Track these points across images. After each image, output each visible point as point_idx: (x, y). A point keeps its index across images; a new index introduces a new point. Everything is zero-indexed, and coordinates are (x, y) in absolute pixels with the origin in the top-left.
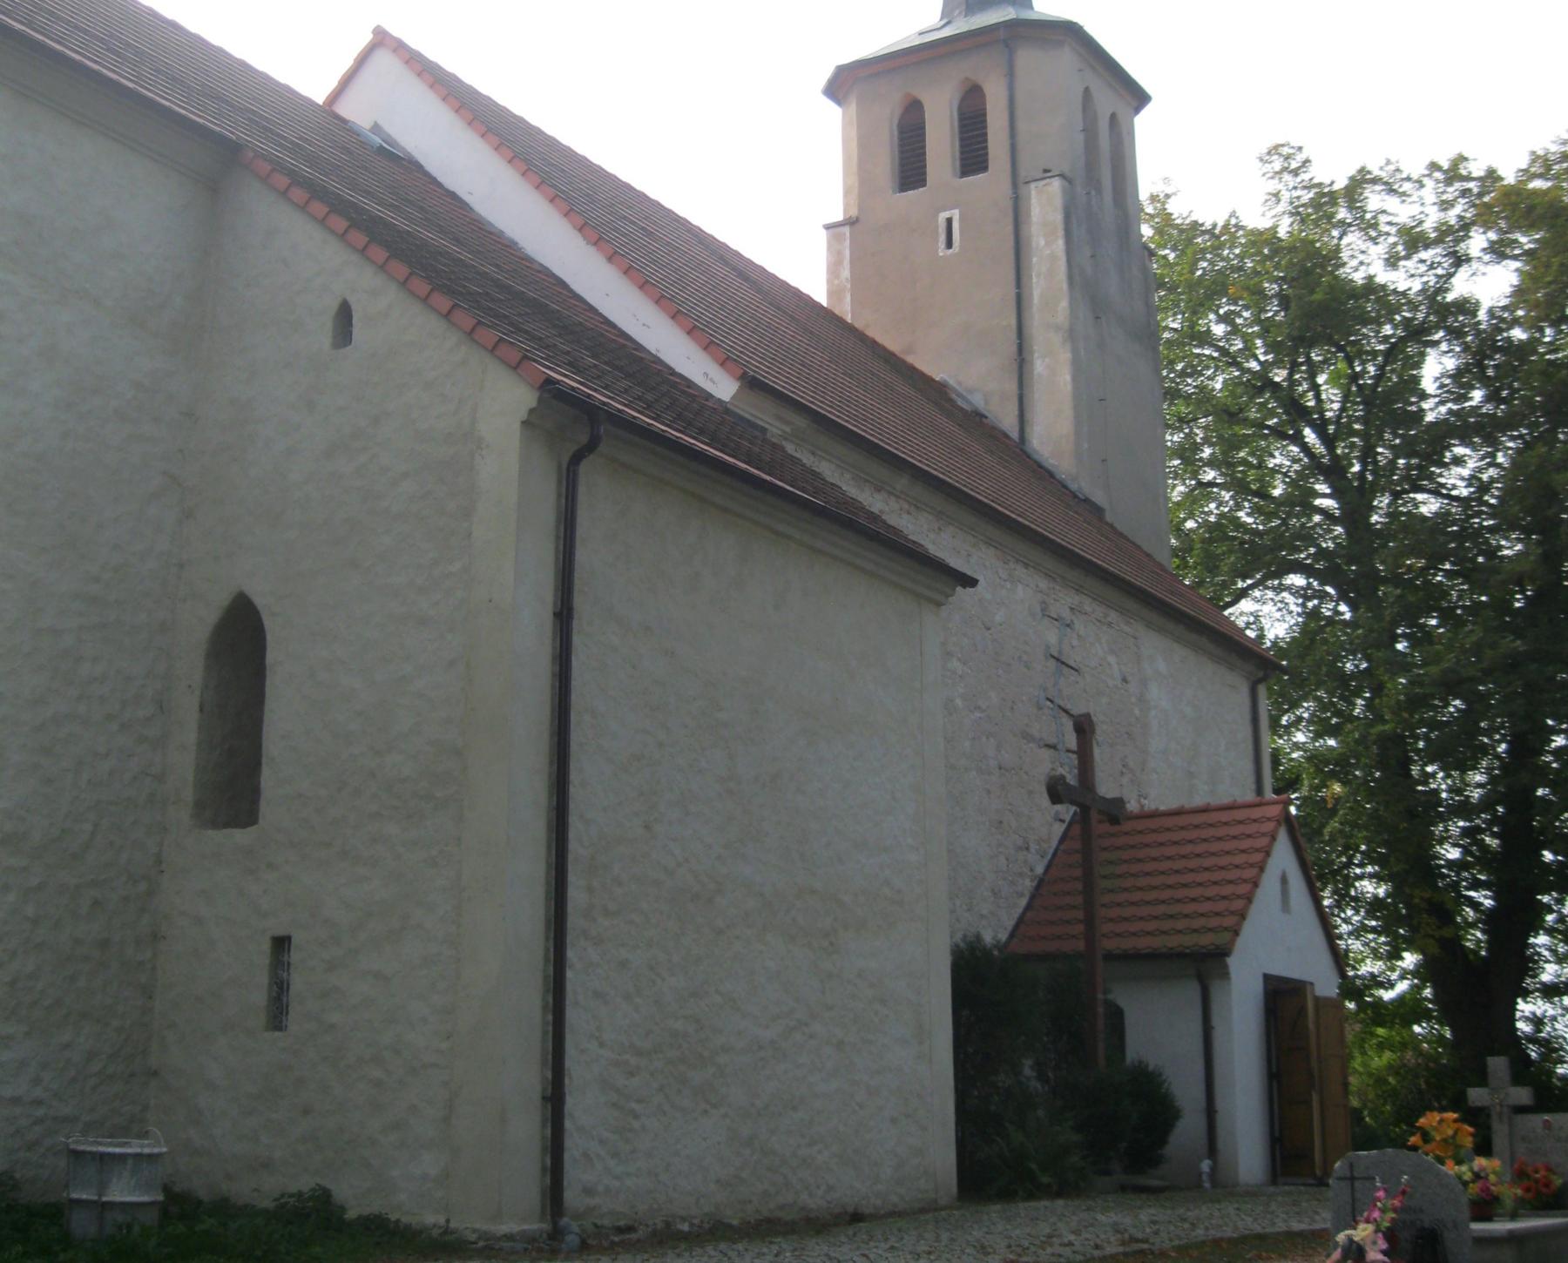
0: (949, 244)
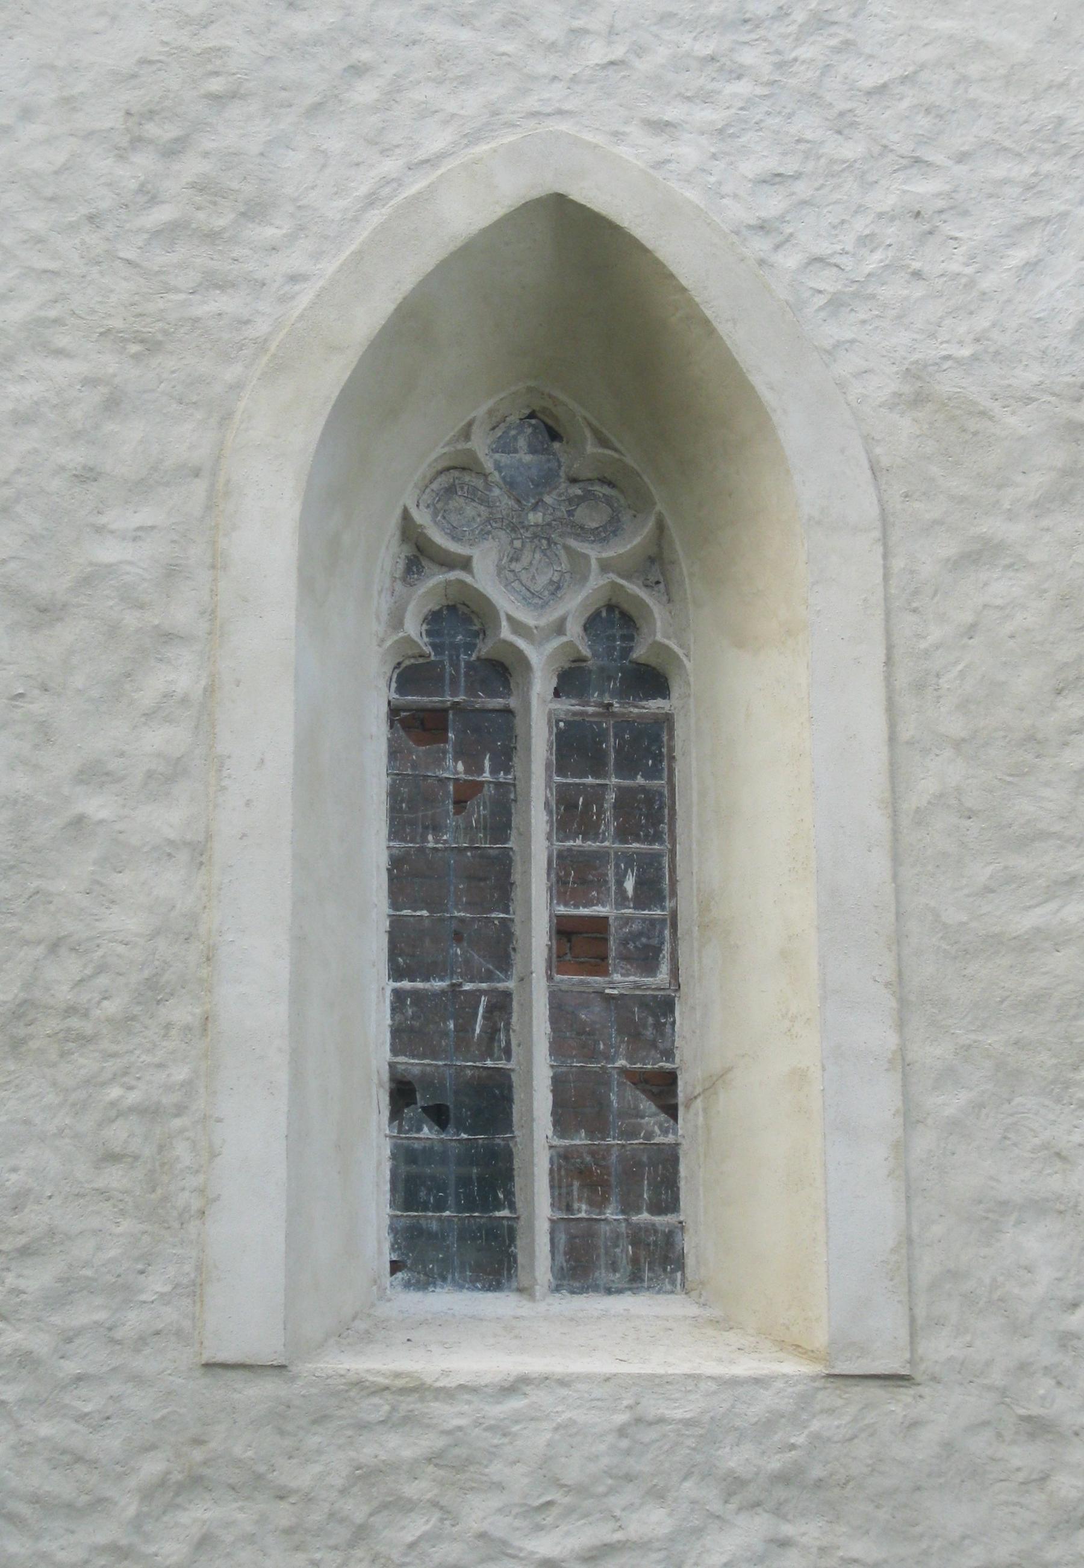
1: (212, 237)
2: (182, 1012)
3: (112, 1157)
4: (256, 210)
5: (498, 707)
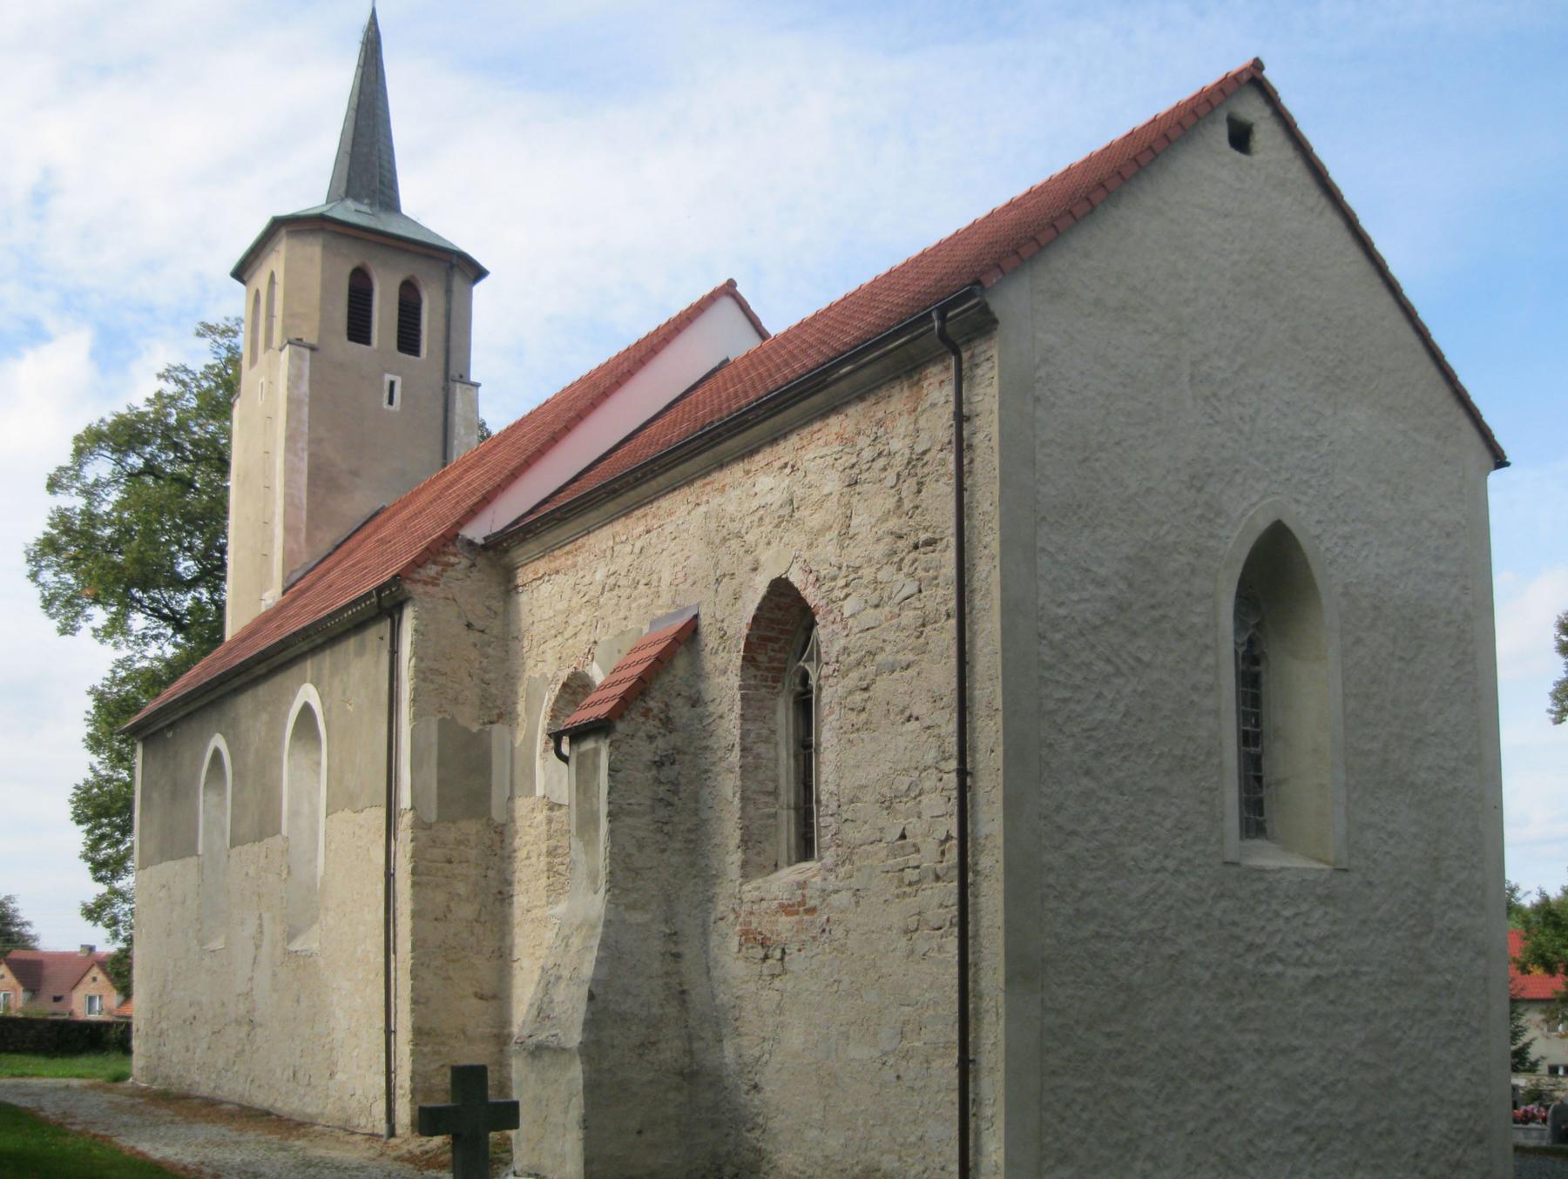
0: (391, 402)
1: (1210, 521)
2: (1215, 761)
3: (1202, 802)
4: (1218, 514)
5: (205, 1131)
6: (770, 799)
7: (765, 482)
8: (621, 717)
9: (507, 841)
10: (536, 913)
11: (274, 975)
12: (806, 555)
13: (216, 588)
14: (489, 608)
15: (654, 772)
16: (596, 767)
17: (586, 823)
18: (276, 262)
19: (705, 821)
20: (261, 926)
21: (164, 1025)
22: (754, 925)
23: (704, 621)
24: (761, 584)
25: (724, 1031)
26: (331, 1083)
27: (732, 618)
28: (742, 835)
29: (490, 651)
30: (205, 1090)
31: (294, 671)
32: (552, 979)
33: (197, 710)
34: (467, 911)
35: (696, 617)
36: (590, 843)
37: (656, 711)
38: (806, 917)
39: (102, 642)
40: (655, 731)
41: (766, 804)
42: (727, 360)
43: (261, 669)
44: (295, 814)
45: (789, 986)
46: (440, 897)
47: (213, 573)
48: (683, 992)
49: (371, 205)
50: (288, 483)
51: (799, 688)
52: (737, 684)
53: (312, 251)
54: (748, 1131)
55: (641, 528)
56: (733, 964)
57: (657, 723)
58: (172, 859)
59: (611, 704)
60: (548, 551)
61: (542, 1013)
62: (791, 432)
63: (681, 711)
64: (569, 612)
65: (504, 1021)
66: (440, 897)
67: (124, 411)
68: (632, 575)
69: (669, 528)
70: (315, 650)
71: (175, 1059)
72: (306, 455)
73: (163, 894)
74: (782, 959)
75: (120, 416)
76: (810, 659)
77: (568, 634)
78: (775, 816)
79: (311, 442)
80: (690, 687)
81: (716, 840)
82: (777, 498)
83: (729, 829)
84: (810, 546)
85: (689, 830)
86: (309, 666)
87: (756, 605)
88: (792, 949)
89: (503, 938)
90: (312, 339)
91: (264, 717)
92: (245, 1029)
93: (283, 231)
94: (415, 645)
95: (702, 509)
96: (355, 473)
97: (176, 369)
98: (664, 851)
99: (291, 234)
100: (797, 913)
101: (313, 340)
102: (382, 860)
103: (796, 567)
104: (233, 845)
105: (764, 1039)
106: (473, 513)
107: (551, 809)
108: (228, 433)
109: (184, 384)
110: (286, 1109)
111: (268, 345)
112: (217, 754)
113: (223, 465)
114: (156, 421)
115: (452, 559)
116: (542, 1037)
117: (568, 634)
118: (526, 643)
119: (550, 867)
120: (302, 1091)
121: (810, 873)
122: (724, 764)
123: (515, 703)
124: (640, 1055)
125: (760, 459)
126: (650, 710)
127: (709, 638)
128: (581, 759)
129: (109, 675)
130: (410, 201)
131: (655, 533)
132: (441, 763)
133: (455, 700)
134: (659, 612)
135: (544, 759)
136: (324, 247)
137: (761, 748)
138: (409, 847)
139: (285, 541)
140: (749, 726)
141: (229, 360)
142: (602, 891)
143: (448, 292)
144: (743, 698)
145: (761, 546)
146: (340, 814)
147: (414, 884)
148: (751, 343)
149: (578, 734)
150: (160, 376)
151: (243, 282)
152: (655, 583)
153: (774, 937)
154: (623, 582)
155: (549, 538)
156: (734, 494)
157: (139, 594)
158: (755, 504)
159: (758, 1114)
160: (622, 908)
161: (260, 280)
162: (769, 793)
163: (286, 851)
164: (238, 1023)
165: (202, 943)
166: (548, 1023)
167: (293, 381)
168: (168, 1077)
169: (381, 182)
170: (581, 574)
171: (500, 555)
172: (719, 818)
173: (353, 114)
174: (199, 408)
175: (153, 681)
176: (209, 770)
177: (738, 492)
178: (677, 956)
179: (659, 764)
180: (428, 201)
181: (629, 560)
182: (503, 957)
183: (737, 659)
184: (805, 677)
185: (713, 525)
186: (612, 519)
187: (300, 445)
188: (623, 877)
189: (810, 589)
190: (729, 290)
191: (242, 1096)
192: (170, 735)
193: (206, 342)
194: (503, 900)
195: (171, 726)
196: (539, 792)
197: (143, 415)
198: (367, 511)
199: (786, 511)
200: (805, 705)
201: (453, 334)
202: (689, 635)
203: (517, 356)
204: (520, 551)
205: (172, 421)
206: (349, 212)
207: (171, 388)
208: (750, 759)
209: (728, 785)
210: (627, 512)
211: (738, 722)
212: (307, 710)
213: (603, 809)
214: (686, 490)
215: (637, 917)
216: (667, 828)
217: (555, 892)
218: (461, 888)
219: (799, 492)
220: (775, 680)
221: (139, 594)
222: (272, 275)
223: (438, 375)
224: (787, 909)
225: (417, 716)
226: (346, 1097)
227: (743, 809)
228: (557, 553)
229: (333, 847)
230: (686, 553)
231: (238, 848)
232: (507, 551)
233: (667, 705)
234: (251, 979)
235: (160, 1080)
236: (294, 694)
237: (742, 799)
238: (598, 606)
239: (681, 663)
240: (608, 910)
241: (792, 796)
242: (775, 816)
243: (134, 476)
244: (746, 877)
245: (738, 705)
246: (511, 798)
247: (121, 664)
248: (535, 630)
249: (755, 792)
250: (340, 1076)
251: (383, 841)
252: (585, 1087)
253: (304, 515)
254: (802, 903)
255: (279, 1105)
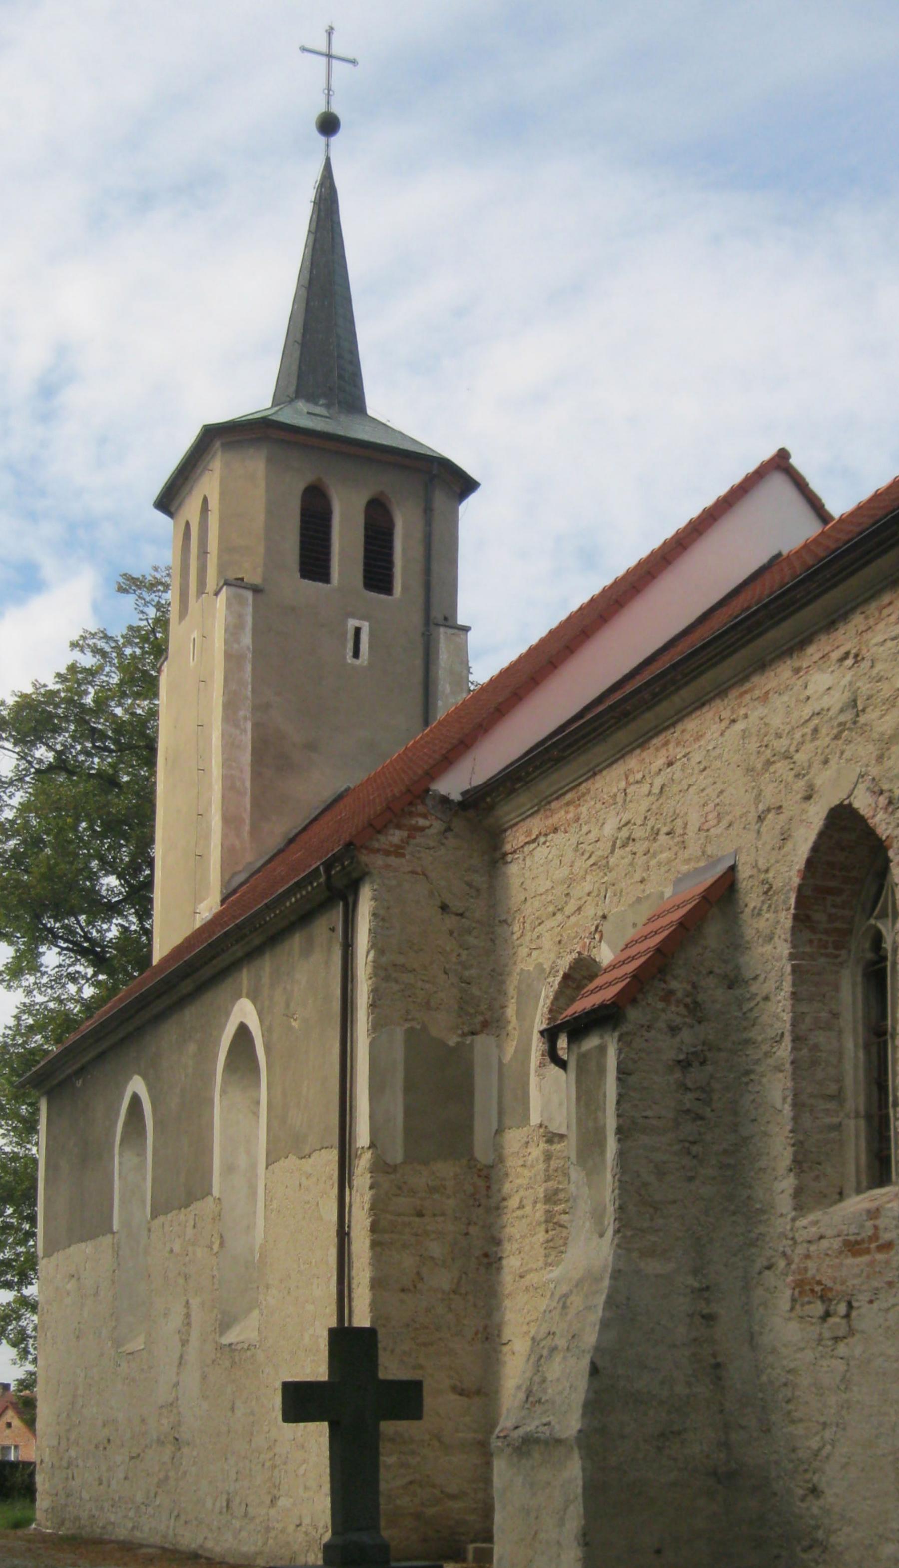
0: (356, 654)
6: (832, 1105)
7: (819, 680)
8: (634, 1001)
9: (495, 1188)
10: (533, 1278)
11: (204, 1377)
12: (874, 771)
13: (145, 914)
14: (470, 885)
15: (678, 1075)
16: (602, 1071)
17: (590, 1143)
18: (209, 485)
19: (746, 1140)
20: (188, 1316)
21: (73, 1453)
22: (810, 1274)
23: (744, 873)
24: (815, 817)
25: (773, 1418)
26: (272, 1512)
27: (778, 862)
28: (795, 1153)
29: (472, 940)
30: (122, 1533)
31: (227, 986)
32: (545, 1352)
33: (114, 1047)
34: (443, 1280)
35: (733, 869)
36: (593, 1171)
37: (680, 994)
38: (880, 1257)
39: (9, 987)
40: (678, 1020)
41: (827, 1111)
42: (779, 555)
43: (187, 986)
44: (229, 1169)
45: (857, 1352)
46: (408, 1262)
47: (140, 896)
48: (717, 1366)
49: (328, 406)
50: (228, 761)
51: (869, 955)
52: (786, 952)
53: (255, 464)
54: (805, 1550)
55: (660, 761)
56: (786, 1330)
57: (682, 1010)
58: (83, 1240)
59: (621, 985)
60: (543, 804)
61: (532, 1398)
62: (853, 610)
63: (714, 994)
64: (570, 881)
65: (489, 1422)
66: (408, 1262)
67: (29, 690)
68: (650, 823)
69: (696, 757)
70: (253, 954)
71: (86, 1496)
72: (249, 726)
73: (71, 1286)
74: (847, 1316)
75: (24, 696)
76: (883, 915)
77: (570, 908)
78: (838, 1127)
79: (255, 708)
80: (726, 962)
81: (762, 1163)
82: (836, 700)
83: (779, 1149)
84: (880, 758)
85: (725, 1152)
86: (245, 977)
87: (809, 844)
88: (860, 1301)
89: (489, 1315)
90: (255, 579)
91: (192, 1048)
92: (168, 1450)
93: (218, 444)
94: (373, 933)
95: (739, 726)
96: (311, 746)
97: (93, 635)
98: (691, 1179)
99: (227, 446)
100: (867, 1251)
101: (257, 580)
102: (334, 1217)
103: (861, 787)
104: (154, 1216)
105: (824, 1425)
106: (448, 759)
107: (550, 1141)
108: (153, 713)
109: (104, 654)
110: (218, 1549)
111: (201, 590)
112: (136, 1100)
113: (147, 751)
114: (70, 701)
115: (421, 822)
116: (530, 1427)
117: (570, 908)
118: (516, 928)
119: (549, 1218)
120: (237, 1523)
121: (885, 1199)
122: (771, 1061)
123: (503, 1007)
124: (660, 1449)
125: (813, 652)
126: (671, 992)
127: (750, 896)
128: (583, 1059)
129: (12, 1022)
130: (377, 403)
131: (678, 765)
132: (408, 1088)
133: (427, 1006)
134: (685, 868)
135: (541, 1076)
136: (269, 460)
137: (820, 1037)
138: (368, 1196)
139: (224, 836)
140: (803, 1008)
141: (157, 620)
142: (610, 1233)
143: (428, 511)
144: (795, 969)
145: (816, 765)
146: (282, 1163)
147: (374, 1245)
148: (810, 529)
149: (579, 1028)
150: (74, 645)
151: (171, 514)
152: (679, 831)
153: (838, 1287)
154: (639, 833)
155: (544, 786)
156: (778, 702)
157: (51, 923)
158: (807, 711)
159: (817, 1527)
160: (635, 1255)
161: (191, 510)
162: (831, 1097)
163: (218, 1217)
164: (161, 1442)
165: (118, 1343)
166: (539, 1409)
167: (233, 632)
168: (78, 1518)
169: (340, 376)
170: (585, 829)
171: (484, 817)
172: (765, 1134)
173: (303, 292)
174: (122, 682)
175: (58, 1023)
176: (126, 1124)
177: (785, 698)
178: (709, 1318)
179: (684, 1065)
180: (398, 403)
181: (645, 804)
182: (490, 1338)
183: (786, 920)
184: (877, 939)
185: (753, 745)
186: (622, 754)
187: (241, 713)
188: (638, 1214)
189: (880, 816)
190: (780, 463)
191: (165, 1536)
192: (79, 1083)
193: (130, 600)
194: (490, 1265)
195: (81, 1071)
196: (535, 1118)
197: (53, 694)
198: (327, 795)
199: (847, 716)
200: (876, 976)
201: (435, 567)
202: (723, 893)
203: (508, 591)
204: (507, 808)
205: (89, 700)
206: (301, 415)
207: (88, 660)
208: (805, 1051)
209: (776, 1089)
210: (642, 741)
211: (788, 1003)
212: (243, 1031)
213: (611, 1123)
214: (718, 704)
215: (653, 1267)
216: (695, 1149)
217: (555, 1248)
218: (435, 1249)
219: (864, 687)
220: (838, 946)
221: (51, 923)
222: (205, 500)
223: (416, 618)
224: (853, 1247)
225: (376, 1026)
226: (291, 1528)
227: (795, 1118)
228: (554, 805)
229: (275, 1205)
230: (719, 786)
231: (162, 1219)
232: (491, 808)
233: (694, 986)
234: (176, 1385)
235: (68, 1524)
236: (228, 1014)
237: (794, 1105)
238: (608, 868)
239: (713, 931)
240: (617, 1257)
241: (861, 1099)
242: (838, 1127)
243: (44, 773)
244: (800, 1208)
245: (787, 986)
246: (500, 1131)
247: (27, 1009)
248: (528, 909)
249: (811, 1095)
250: (282, 1502)
251: (335, 1191)
252: (585, 1488)
253: (247, 801)
254: (874, 1237)
255: (210, 1544)
